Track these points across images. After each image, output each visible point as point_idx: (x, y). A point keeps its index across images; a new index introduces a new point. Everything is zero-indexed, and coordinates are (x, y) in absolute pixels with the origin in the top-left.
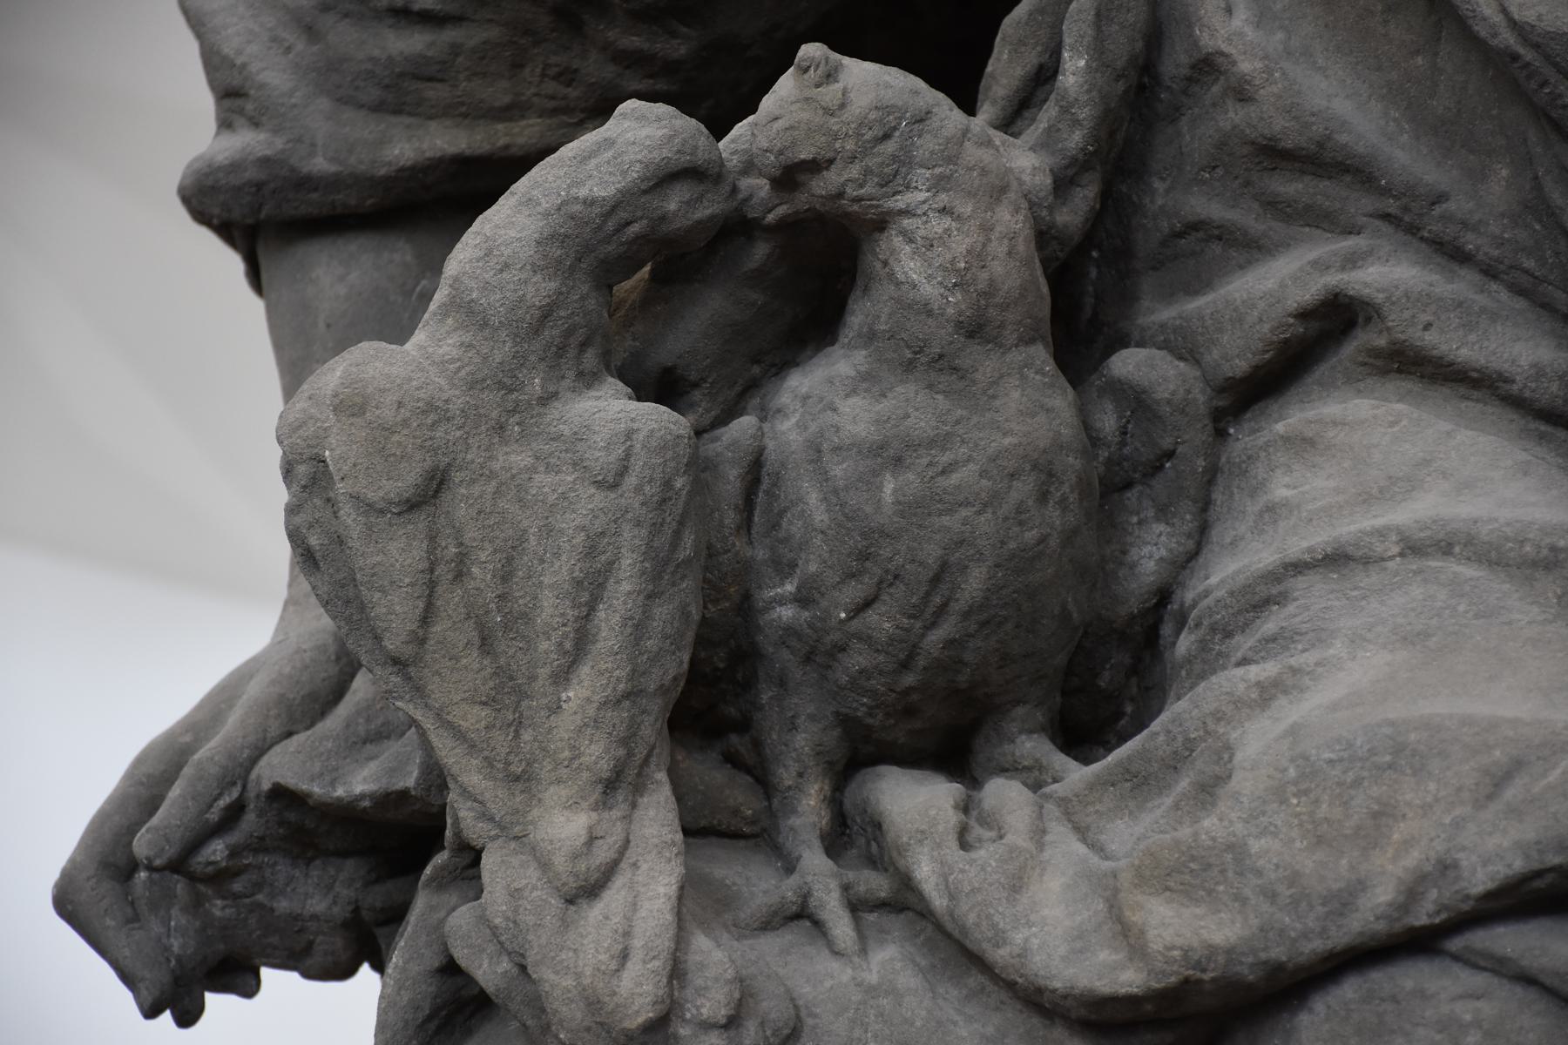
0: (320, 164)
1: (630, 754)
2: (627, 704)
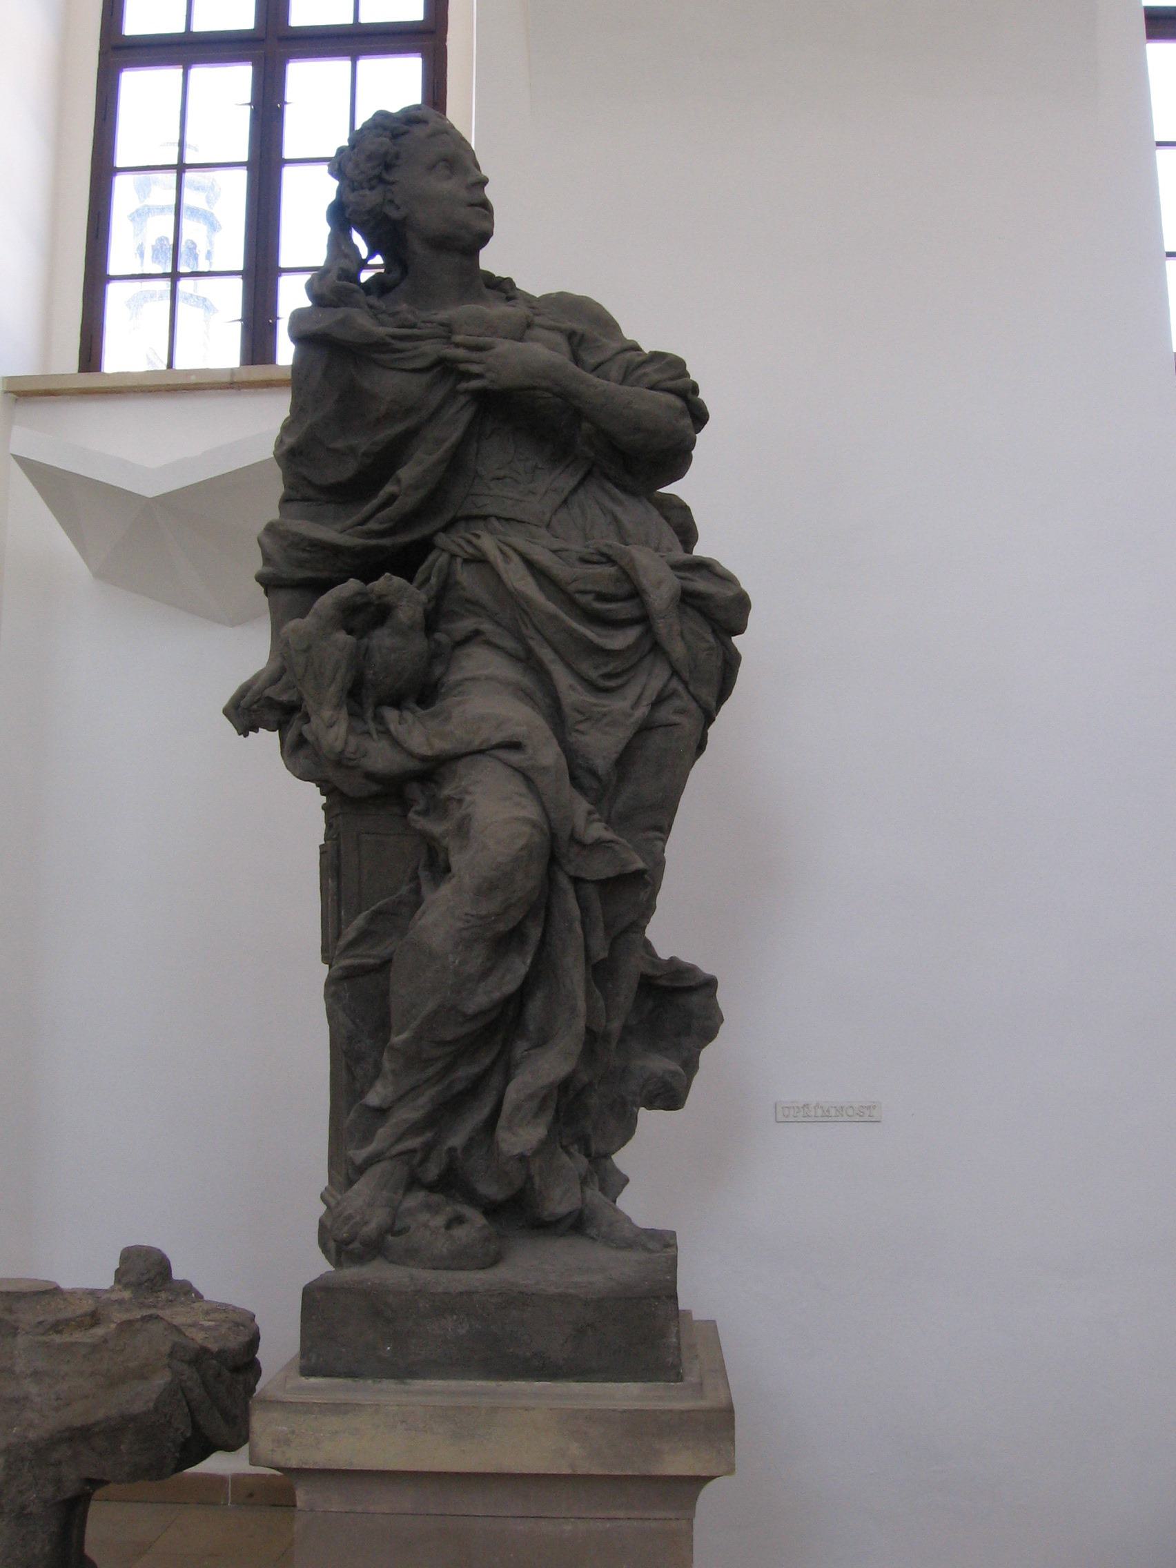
0: (284, 576)
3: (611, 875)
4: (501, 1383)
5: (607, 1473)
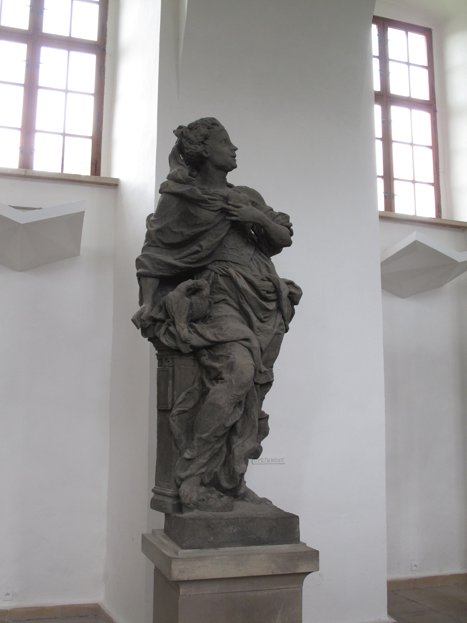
0: (153, 273)
3: (266, 382)
4: (247, 547)
5: (283, 573)
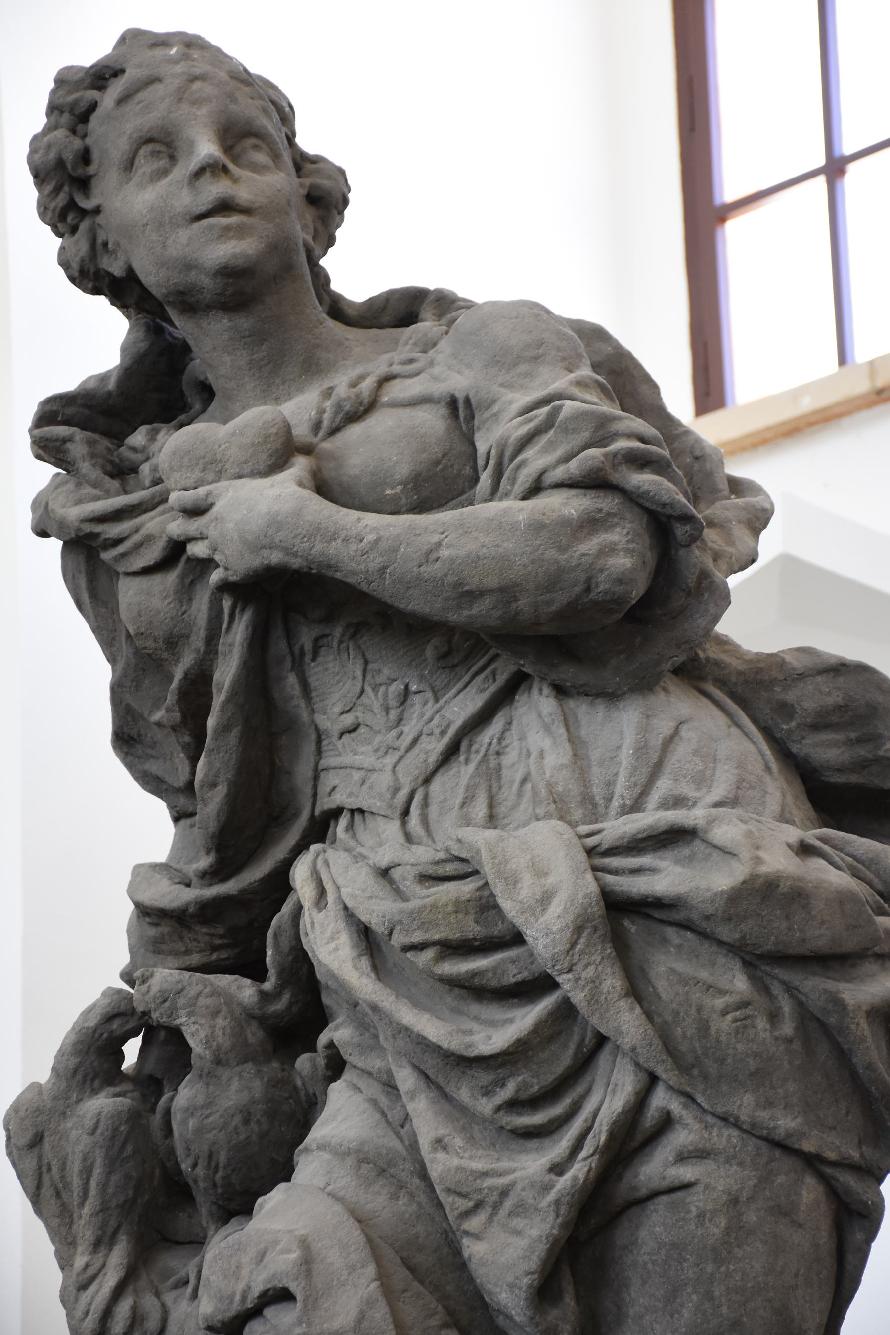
1: (104, 1232)
2: (101, 1214)
